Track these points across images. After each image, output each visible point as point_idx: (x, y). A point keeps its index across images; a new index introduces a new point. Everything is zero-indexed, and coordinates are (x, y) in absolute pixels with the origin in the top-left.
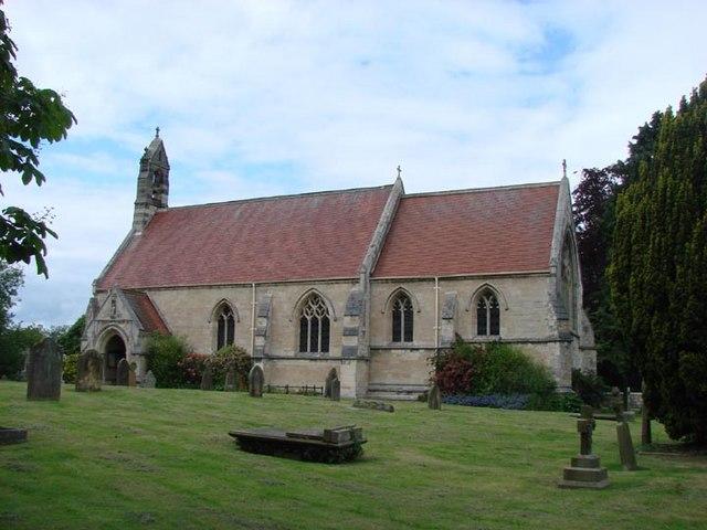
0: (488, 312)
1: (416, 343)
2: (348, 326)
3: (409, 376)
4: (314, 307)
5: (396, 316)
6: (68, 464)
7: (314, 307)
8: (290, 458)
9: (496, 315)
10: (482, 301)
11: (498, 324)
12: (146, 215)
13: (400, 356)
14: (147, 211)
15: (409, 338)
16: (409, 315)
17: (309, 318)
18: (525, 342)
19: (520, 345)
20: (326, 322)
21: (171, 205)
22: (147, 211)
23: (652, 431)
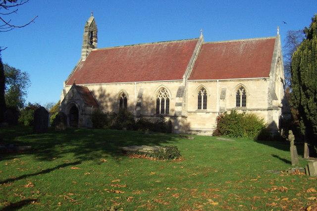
0: (241, 99)
1: (208, 110)
2: (177, 102)
3: (204, 125)
4: (163, 94)
5: (200, 98)
6: (40, 157)
7: (163, 94)
8: (264, 144)
9: (244, 97)
10: (238, 91)
11: (245, 102)
12: (87, 52)
13: (202, 115)
14: (88, 50)
15: (205, 107)
16: (205, 97)
17: (160, 99)
18: (257, 110)
19: (260, 111)
20: (168, 101)
21: (26, 104)
22: (88, 50)
23: (73, 162)
